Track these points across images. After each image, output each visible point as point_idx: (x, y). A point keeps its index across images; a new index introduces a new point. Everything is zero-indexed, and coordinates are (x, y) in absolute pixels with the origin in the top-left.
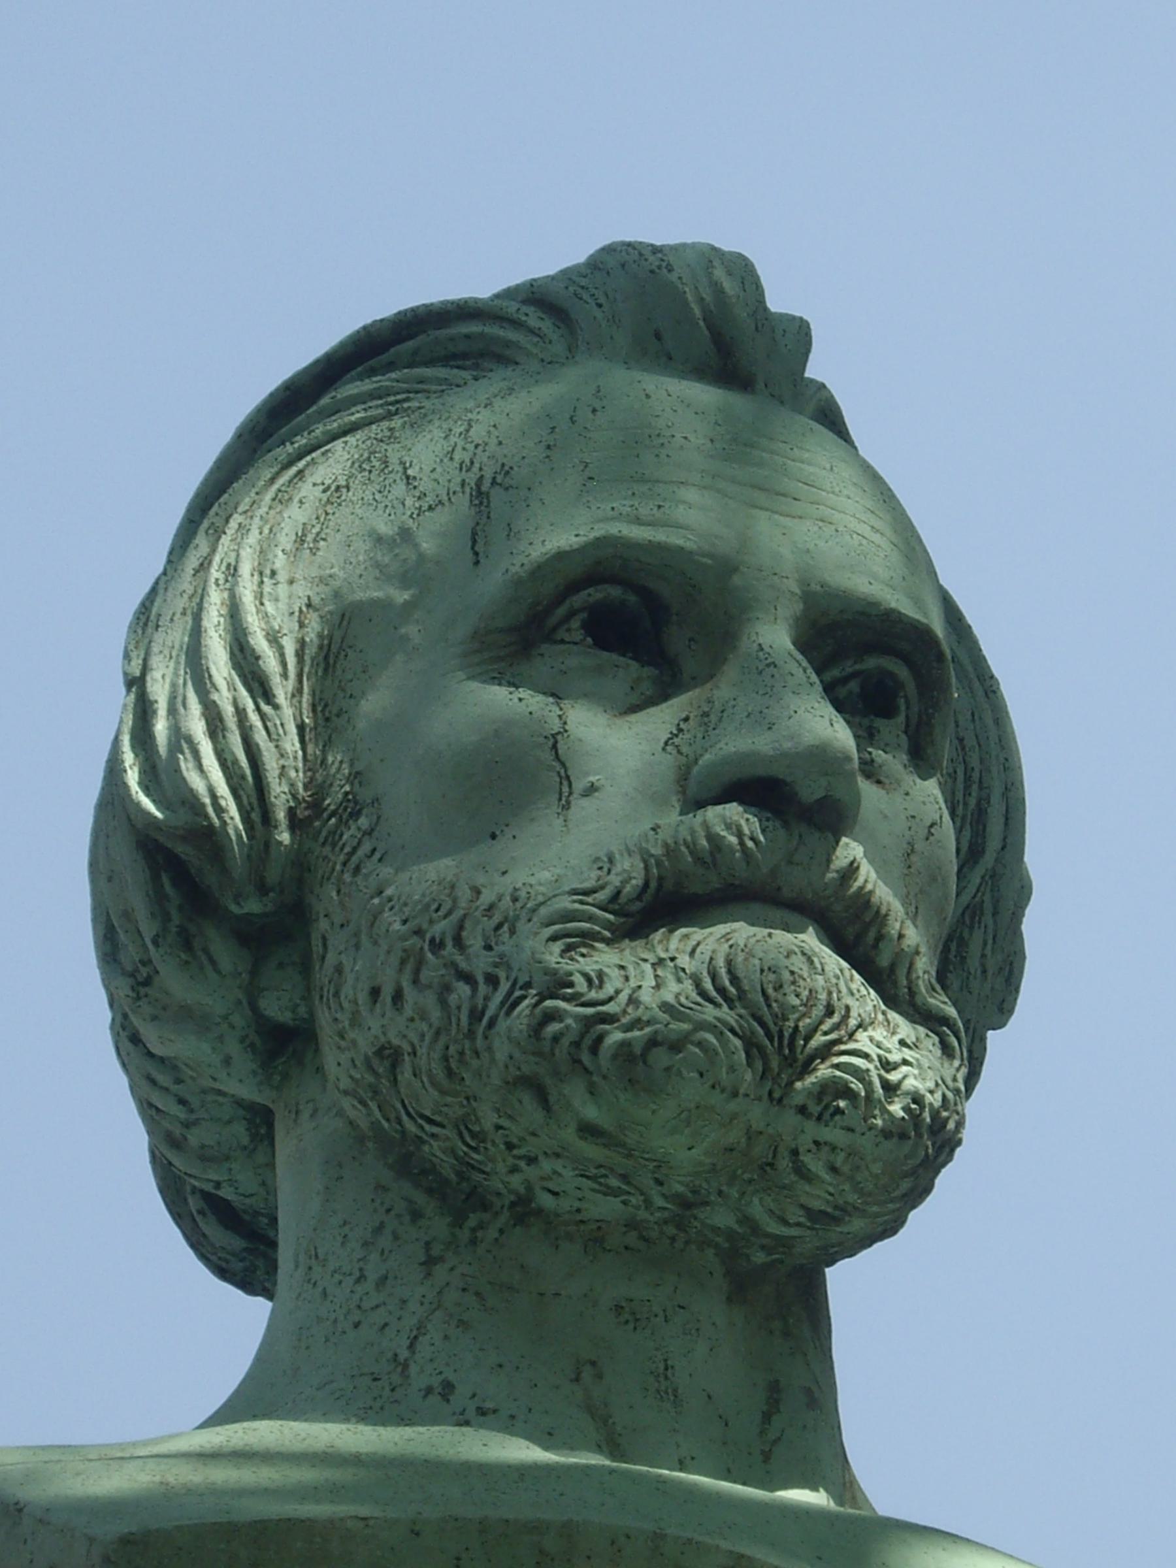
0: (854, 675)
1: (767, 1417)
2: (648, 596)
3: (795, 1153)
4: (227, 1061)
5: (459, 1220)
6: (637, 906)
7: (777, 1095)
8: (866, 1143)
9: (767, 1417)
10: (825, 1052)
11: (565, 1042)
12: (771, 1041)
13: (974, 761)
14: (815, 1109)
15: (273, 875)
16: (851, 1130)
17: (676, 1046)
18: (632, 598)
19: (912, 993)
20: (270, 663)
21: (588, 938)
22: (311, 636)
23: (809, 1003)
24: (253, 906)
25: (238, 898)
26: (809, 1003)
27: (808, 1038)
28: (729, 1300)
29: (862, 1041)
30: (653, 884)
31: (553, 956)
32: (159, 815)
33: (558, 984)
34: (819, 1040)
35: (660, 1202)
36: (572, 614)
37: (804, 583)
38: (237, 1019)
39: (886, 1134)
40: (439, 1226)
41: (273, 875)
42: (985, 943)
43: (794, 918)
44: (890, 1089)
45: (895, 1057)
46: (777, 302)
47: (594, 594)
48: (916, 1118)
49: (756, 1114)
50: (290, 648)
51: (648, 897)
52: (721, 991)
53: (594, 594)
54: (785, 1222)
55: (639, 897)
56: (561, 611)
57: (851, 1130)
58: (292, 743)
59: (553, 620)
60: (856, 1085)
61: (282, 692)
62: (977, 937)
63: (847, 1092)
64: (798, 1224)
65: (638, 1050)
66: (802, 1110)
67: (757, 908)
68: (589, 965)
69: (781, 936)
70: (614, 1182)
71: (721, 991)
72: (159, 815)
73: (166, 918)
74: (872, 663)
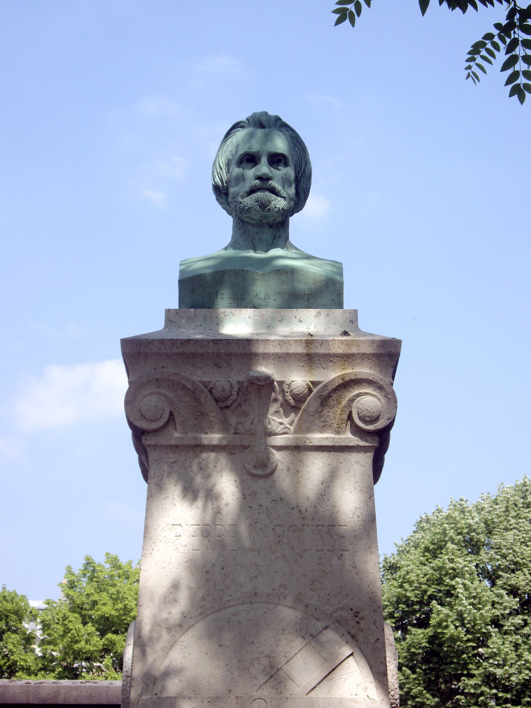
1: (273, 240)
5: (243, 224)
8: (274, 214)
9: (273, 240)
10: (268, 205)
15: (225, 188)
17: (251, 208)
18: (248, 156)
20: (222, 166)
21: (244, 197)
22: (226, 162)
23: (265, 201)
24: (224, 192)
26: (265, 201)
28: (269, 228)
31: (240, 200)
32: (524, 23)
33: (241, 203)
34: (267, 204)
37: (267, 151)
39: (276, 212)
40: (241, 225)
41: (225, 188)
43: (265, 191)
44: (275, 208)
45: (276, 204)
47: (246, 157)
48: (279, 210)
49: (262, 213)
50: (224, 164)
53: (246, 157)
58: (225, 174)
60: (272, 208)
61: (223, 169)
62: (302, 179)
63: (271, 209)
67: (261, 191)
68: (244, 200)
69: (263, 193)
72: (524, 23)
74: (277, 158)
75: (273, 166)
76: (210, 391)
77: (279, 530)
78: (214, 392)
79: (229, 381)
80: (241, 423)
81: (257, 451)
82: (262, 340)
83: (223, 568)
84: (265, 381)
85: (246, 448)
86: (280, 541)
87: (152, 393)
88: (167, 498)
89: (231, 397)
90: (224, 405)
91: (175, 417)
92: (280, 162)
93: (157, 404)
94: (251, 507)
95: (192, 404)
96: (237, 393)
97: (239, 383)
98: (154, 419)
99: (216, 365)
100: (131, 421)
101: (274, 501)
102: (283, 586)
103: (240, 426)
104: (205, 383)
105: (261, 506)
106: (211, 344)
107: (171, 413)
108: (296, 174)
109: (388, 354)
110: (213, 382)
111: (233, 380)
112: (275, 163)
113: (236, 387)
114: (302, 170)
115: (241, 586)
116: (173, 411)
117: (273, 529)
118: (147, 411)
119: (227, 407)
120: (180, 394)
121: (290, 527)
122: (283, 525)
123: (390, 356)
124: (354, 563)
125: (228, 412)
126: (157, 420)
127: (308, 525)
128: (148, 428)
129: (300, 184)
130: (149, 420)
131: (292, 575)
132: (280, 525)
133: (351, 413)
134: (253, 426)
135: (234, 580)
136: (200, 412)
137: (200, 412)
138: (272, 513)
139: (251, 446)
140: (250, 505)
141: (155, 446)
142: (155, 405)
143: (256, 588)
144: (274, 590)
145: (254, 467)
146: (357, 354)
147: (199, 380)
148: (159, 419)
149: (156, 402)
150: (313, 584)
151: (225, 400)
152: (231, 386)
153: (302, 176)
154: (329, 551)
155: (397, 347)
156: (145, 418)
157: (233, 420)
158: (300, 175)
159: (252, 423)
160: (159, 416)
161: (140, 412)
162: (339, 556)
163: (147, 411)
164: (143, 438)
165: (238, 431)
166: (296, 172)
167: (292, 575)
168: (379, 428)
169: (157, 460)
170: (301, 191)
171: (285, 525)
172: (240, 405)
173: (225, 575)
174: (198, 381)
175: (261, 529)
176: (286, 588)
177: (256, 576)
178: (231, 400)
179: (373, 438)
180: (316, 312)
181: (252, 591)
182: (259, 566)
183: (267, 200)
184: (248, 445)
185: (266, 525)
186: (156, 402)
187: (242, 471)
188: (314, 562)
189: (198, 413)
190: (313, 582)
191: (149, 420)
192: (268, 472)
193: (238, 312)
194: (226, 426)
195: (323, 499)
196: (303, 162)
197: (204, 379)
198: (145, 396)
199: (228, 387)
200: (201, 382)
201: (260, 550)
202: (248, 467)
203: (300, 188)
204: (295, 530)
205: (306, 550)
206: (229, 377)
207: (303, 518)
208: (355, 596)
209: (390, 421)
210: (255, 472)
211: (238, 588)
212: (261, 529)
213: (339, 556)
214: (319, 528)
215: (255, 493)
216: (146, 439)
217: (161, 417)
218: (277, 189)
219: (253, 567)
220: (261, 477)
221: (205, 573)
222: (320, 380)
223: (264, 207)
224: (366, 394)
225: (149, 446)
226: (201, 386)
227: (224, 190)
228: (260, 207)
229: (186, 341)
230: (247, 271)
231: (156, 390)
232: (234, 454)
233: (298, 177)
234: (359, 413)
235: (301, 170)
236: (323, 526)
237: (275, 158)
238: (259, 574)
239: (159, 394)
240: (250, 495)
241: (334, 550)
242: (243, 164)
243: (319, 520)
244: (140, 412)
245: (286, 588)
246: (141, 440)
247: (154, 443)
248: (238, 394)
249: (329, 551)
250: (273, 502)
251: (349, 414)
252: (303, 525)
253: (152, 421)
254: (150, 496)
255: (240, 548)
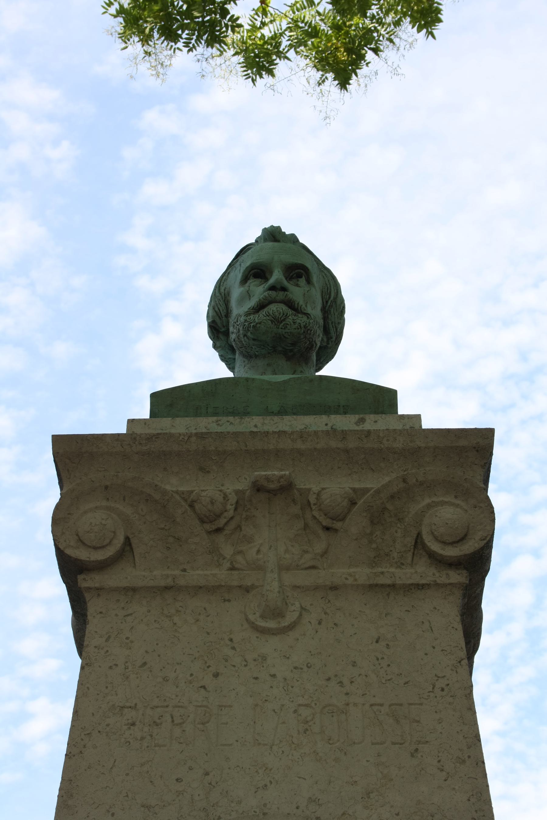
0: (295, 273)
2: (261, 270)
3: (283, 335)
4: (227, 352)
6: (257, 308)
7: (278, 327)
11: (247, 328)
12: (275, 319)
13: (329, 286)
14: (283, 328)
16: (289, 329)
18: (259, 271)
19: (301, 311)
23: (280, 314)
25: (221, 329)
27: (280, 318)
29: (290, 317)
30: (259, 305)
34: (282, 318)
35: (270, 348)
36: (251, 275)
38: (226, 346)
42: (334, 310)
46: (283, 231)
51: (259, 307)
52: (267, 315)
54: (288, 347)
55: (257, 307)
56: (249, 275)
57: (289, 329)
59: (249, 277)
60: (288, 323)
63: (288, 324)
64: (290, 346)
65: (255, 326)
66: (282, 328)
70: (262, 347)
71: (267, 315)
73: (214, 335)
75: (291, 282)
76: (191, 506)
77: (305, 713)
78: (197, 506)
79: (221, 491)
80: (241, 552)
81: (267, 591)
82: (274, 432)
83: (207, 774)
84: (279, 481)
85: (248, 590)
86: (307, 730)
87: (96, 507)
88: (114, 667)
89: (226, 514)
90: (214, 527)
91: (134, 545)
92: (301, 277)
93: (104, 522)
94: (256, 678)
95: (162, 526)
96: (234, 506)
97: (237, 492)
98: (98, 545)
99: (202, 469)
100: (62, 547)
101: (296, 668)
102: (314, 801)
103: (239, 558)
104: (183, 493)
105: (274, 676)
106: (193, 439)
107: (128, 541)
108: (323, 302)
109: (475, 448)
110: (196, 492)
111: (228, 489)
112: (293, 278)
113: (233, 499)
114: (332, 298)
115: (239, 802)
116: (130, 536)
117: (295, 711)
118: (88, 532)
119: (219, 530)
120: (142, 510)
121: (324, 707)
122: (313, 705)
123: (477, 451)
124: (439, 761)
125: (220, 539)
126: (102, 547)
127: (355, 704)
128: (88, 559)
129: (330, 316)
130: (90, 547)
131: (330, 782)
132: (307, 705)
133: (419, 535)
134: (261, 556)
135: (227, 792)
136: (174, 537)
137: (174, 537)
138: (292, 687)
139: (257, 587)
140: (255, 675)
141: (99, 590)
142: (101, 523)
143: (265, 805)
144: (297, 808)
145: (263, 617)
146: (425, 448)
147: (174, 489)
148: (107, 545)
149: (103, 519)
150: (369, 797)
151: (215, 520)
152: (225, 497)
153: (331, 306)
154: (394, 743)
155: (488, 438)
156: (84, 544)
157: (228, 551)
158: (329, 304)
159: (258, 551)
160: (107, 541)
161: (77, 535)
162: (412, 751)
163: (88, 532)
164: (80, 577)
165: (237, 566)
166: (323, 300)
167: (330, 782)
168: (468, 552)
169: (101, 613)
170: (331, 326)
171: (316, 704)
172: (239, 527)
173: (210, 784)
174: (172, 491)
175: (274, 711)
176: (320, 805)
177: (266, 786)
178: (225, 518)
179: (458, 572)
180: (357, 419)
181: (257, 810)
182: (271, 770)
183: (282, 312)
184: (253, 585)
185: (283, 705)
186: (103, 519)
187: (242, 625)
188: (368, 761)
189: (171, 540)
190: (368, 794)
191: (90, 547)
192: (286, 624)
193: (238, 420)
194: (216, 558)
195: (380, 664)
196: (332, 289)
197: (181, 489)
198: (85, 512)
199: (219, 498)
200: (177, 492)
201: (273, 745)
202: (251, 617)
203: (330, 322)
204: (333, 712)
205: (354, 743)
206: (222, 485)
207: (347, 694)
208: (446, 817)
209: (485, 541)
210: (262, 623)
211: (233, 805)
212: (274, 711)
213: (412, 751)
214: (375, 708)
215: (264, 658)
216: (84, 579)
217: (110, 543)
218: (296, 303)
219: (260, 771)
220: (273, 634)
221: (175, 782)
222: (368, 486)
223: (278, 322)
224: (443, 503)
225: (89, 589)
226: (178, 497)
227: (224, 327)
228: (272, 321)
229: (154, 435)
230: (253, 379)
231: (104, 503)
232: (229, 601)
233: (326, 307)
234: (433, 531)
235: (330, 298)
236: (381, 705)
237: (294, 272)
238: (271, 782)
239: (108, 508)
240: (255, 660)
241: (403, 742)
242: (249, 282)
243: (374, 696)
244: (77, 535)
245: (320, 805)
246: (76, 582)
247: (97, 585)
248: (236, 509)
249: (394, 743)
250: (294, 670)
251: (418, 536)
252: (348, 704)
253: (95, 548)
254: (87, 664)
255: (237, 741)
